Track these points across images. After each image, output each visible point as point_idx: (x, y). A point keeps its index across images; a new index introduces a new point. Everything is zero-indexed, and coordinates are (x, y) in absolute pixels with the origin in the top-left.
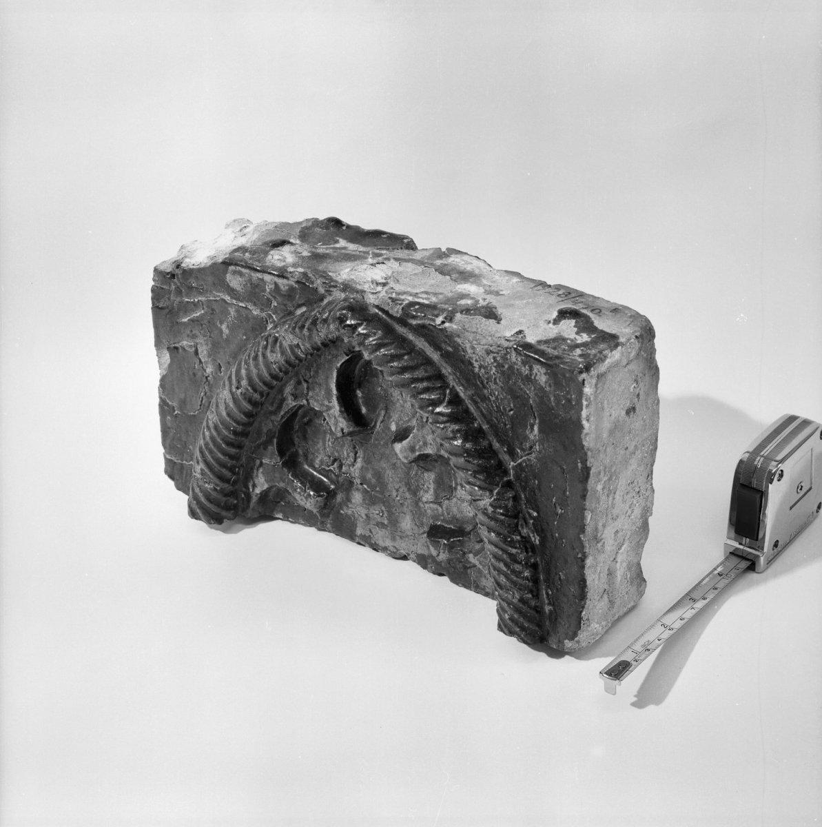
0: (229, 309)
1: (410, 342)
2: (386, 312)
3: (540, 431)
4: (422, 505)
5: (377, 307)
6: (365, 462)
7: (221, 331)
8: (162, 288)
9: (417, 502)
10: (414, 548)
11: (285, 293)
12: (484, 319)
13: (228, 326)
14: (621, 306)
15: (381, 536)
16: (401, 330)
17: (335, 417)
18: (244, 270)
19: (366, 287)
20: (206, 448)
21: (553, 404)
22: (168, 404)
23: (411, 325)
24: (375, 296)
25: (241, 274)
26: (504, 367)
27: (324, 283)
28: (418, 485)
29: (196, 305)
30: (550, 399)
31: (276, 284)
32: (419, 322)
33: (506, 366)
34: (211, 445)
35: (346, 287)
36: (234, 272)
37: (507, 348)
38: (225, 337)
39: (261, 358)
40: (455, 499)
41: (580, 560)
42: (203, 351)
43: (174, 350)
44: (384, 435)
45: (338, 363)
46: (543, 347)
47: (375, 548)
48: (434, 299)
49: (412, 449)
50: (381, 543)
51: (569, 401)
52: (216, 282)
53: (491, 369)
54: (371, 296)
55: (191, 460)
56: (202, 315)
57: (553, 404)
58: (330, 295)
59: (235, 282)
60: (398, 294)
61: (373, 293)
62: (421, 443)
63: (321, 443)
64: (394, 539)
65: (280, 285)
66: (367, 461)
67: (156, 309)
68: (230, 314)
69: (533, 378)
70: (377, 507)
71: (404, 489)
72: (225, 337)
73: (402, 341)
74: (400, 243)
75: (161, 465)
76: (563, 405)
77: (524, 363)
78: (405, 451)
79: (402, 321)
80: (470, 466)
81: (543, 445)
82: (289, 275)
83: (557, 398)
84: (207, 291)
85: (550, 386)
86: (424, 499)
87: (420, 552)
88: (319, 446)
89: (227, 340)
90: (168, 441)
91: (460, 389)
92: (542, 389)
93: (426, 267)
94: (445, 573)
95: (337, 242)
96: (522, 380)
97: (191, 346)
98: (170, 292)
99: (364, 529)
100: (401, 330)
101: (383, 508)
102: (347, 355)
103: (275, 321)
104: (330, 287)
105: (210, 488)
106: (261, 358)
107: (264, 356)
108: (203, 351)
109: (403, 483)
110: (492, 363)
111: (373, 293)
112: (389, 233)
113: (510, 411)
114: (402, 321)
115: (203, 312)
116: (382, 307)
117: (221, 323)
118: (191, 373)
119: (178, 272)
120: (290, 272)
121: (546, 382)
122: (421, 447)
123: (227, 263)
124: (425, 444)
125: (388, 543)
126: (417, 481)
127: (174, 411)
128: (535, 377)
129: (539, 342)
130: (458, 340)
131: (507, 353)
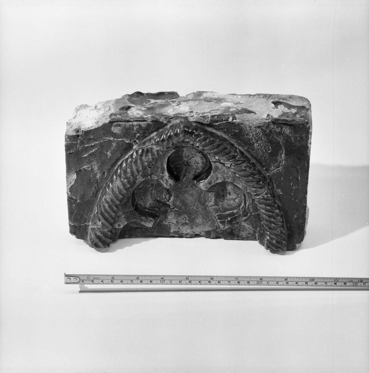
0: (113, 143)
1: (215, 134)
2: (201, 124)
3: (286, 155)
4: (208, 208)
5: (196, 122)
6: (175, 197)
7: (107, 155)
8: (73, 143)
9: (205, 208)
10: (204, 230)
11: (144, 128)
12: (248, 114)
13: (111, 152)
14: (291, 95)
15: (185, 230)
16: (210, 129)
17: (166, 180)
18: (121, 123)
19: (187, 115)
20: (106, 212)
21: (293, 141)
22: (73, 199)
23: (215, 126)
24: (192, 118)
25: (119, 125)
26: (266, 131)
27: (165, 118)
28: (205, 200)
29: (92, 147)
30: (292, 139)
31: (140, 125)
32: (219, 123)
33: (268, 131)
34: (108, 209)
35: (176, 117)
36: (116, 126)
37: (268, 123)
38: (108, 157)
39: (139, 161)
40: (226, 201)
41: (304, 207)
42: (96, 168)
43: (78, 173)
44: (186, 182)
45: (169, 154)
46: (283, 118)
47: (181, 236)
48: (219, 112)
49: (210, 183)
50: (185, 232)
51: (302, 138)
52: (105, 133)
53: (260, 134)
54: (191, 118)
55: (85, 222)
56: (96, 151)
57: (293, 141)
58: (170, 123)
59: (116, 130)
60: (202, 114)
61: (191, 117)
62: (215, 179)
63: (150, 196)
64: (192, 228)
65: (142, 125)
66: (177, 197)
67: (69, 156)
68: (113, 146)
69: (282, 132)
70: (182, 217)
71: (197, 203)
72: (108, 157)
73: (212, 134)
74: (173, 95)
75: (68, 228)
76: (298, 140)
77: (278, 127)
78: (206, 184)
79: (210, 125)
80: (254, 180)
81: (287, 161)
82: (146, 119)
83: (296, 139)
84: (99, 138)
85: (292, 134)
86: (209, 205)
87: (207, 230)
88: (148, 197)
89: (110, 158)
90: (73, 217)
91: (241, 148)
92: (287, 136)
93: (199, 101)
94: (221, 236)
95: (150, 101)
96: (276, 135)
97: (89, 168)
98: (77, 144)
99: (175, 229)
100: (210, 129)
101: (186, 216)
102: (174, 149)
103: (138, 143)
104: (169, 119)
105: (107, 231)
106: (139, 161)
107: (141, 159)
108: (96, 168)
109: (197, 201)
110: (261, 131)
111: (191, 117)
112: (167, 92)
113: (268, 151)
114: (210, 125)
115: (96, 149)
116: (198, 121)
117: (107, 152)
118: (88, 180)
119: (80, 133)
120: (146, 118)
121: (289, 132)
122: (215, 181)
123: (111, 123)
124: (217, 179)
125: (189, 231)
126: (204, 198)
127: (77, 201)
128: (283, 132)
129: (279, 116)
130: (243, 126)
131: (269, 124)
